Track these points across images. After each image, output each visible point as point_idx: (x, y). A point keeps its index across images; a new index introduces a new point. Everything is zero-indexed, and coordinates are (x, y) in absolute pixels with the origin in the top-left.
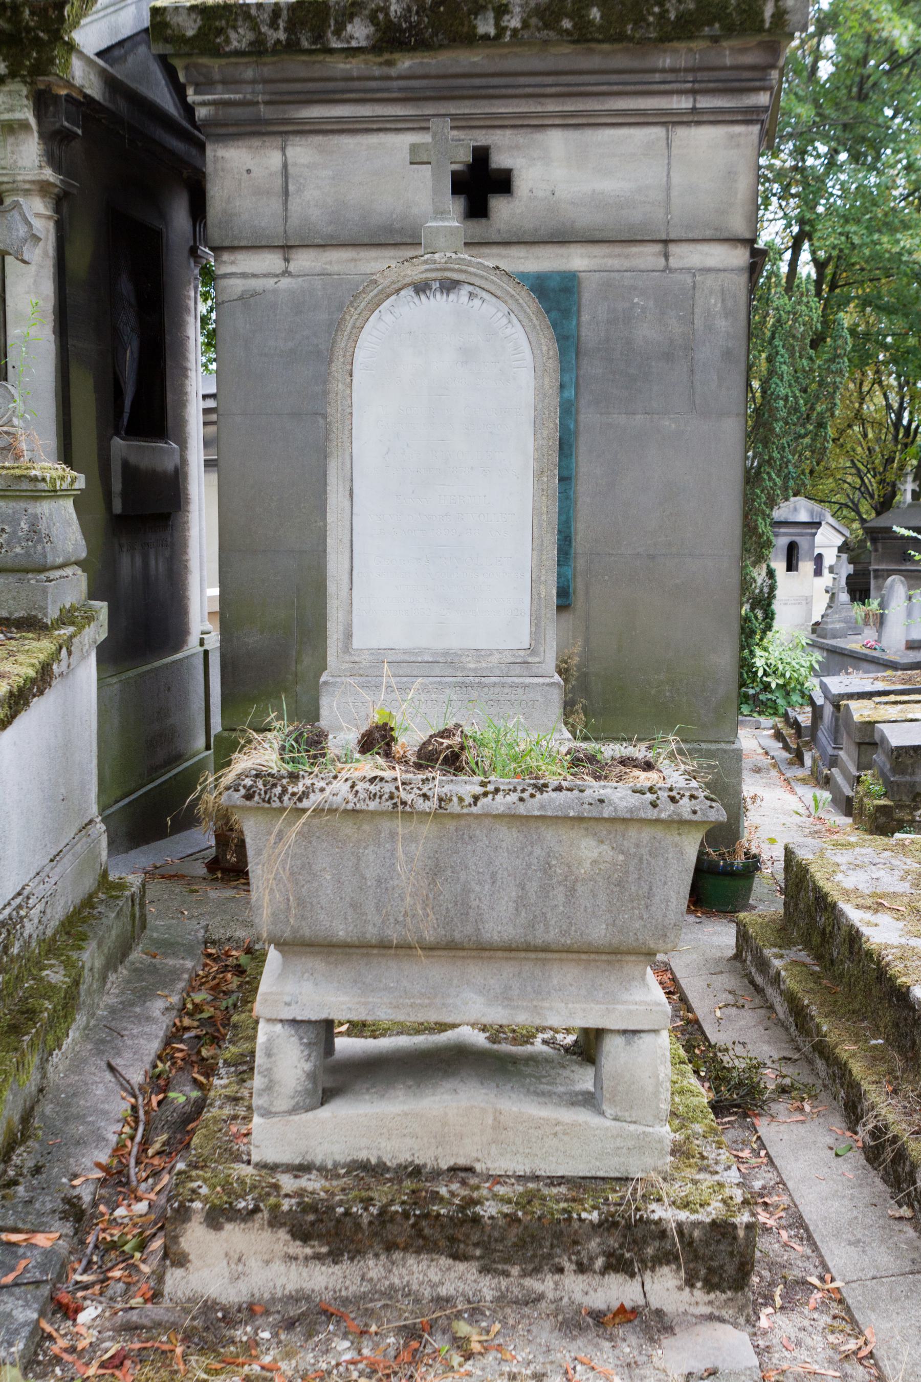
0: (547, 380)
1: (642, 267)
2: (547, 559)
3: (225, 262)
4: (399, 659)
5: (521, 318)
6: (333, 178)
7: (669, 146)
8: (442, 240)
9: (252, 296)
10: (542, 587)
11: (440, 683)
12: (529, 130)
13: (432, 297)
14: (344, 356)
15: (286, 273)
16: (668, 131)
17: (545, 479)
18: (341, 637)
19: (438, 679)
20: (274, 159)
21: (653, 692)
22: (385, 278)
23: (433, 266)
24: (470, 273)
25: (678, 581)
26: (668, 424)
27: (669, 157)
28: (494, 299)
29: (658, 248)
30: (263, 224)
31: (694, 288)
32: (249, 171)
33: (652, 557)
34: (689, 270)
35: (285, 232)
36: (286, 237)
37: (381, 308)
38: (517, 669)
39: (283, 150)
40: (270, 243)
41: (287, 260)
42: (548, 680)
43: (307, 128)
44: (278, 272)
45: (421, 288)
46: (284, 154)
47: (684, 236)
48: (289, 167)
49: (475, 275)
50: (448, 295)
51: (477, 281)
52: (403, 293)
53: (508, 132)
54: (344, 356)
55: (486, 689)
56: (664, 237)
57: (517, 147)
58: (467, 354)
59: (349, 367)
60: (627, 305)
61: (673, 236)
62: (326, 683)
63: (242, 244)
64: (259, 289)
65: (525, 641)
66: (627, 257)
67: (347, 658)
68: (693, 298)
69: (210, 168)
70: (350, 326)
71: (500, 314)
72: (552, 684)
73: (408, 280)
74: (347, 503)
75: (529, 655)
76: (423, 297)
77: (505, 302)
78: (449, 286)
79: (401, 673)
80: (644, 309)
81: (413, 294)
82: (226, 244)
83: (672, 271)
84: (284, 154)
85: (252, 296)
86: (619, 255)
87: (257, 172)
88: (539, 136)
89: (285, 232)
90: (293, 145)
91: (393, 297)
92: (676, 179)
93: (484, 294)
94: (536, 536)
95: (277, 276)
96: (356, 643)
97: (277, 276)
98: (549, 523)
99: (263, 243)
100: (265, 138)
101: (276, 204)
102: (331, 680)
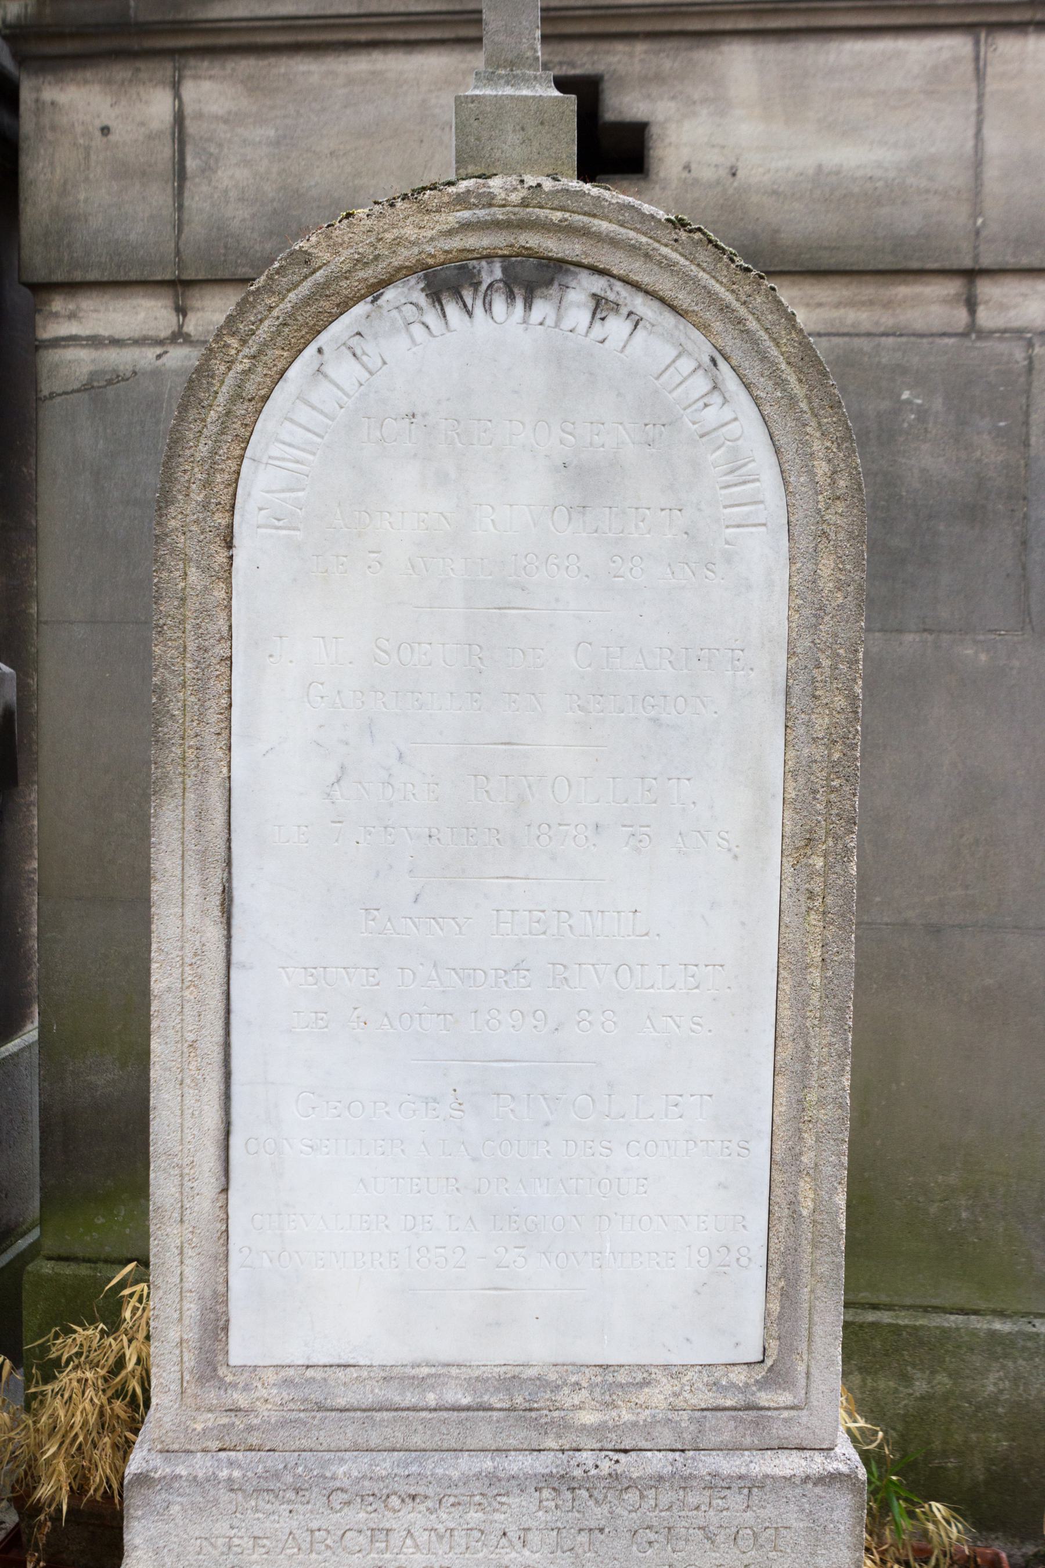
0: (827, 565)
1: (919, 326)
2: (821, 1103)
3: (56, 315)
4: (369, 1400)
5: (752, 375)
6: (278, 143)
7: (979, 75)
8: (513, 138)
9: (110, 382)
10: (805, 1186)
11: (493, 1479)
12: (684, 43)
13: (479, 311)
14: (207, 484)
15: (179, 337)
16: (977, 43)
17: (819, 863)
18: (192, 1335)
19: (487, 1464)
20: (157, 106)
21: (933, 1209)
22: (335, 248)
23: (482, 213)
24: (599, 238)
25: (989, 981)
26: (972, 654)
27: (980, 97)
28: (669, 319)
29: (952, 287)
30: (133, 237)
31: (1030, 369)
32: (105, 130)
33: (935, 930)
34: (1018, 333)
35: (178, 253)
36: (180, 264)
37: (323, 339)
38: (726, 1430)
39: (176, 87)
40: (146, 276)
41: (181, 311)
42: (818, 1464)
43: (225, 40)
44: (163, 334)
45: (447, 282)
46: (177, 95)
47: (1011, 261)
48: (188, 122)
49: (614, 242)
50: (528, 305)
51: (619, 262)
52: (390, 294)
53: (640, 48)
54: (207, 484)
55: (632, 1496)
56: (967, 263)
57: (659, 78)
58: (585, 483)
59: (220, 519)
60: (885, 405)
61: (986, 262)
62: (143, 1479)
63: (93, 276)
64: (125, 368)
65: (748, 1339)
66: (888, 305)
67: (212, 1396)
68: (1028, 392)
69: (27, 124)
70: (224, 392)
71: (686, 365)
72: (833, 1479)
73: (405, 256)
74: (214, 933)
75: (764, 1384)
76: (452, 309)
77: (704, 328)
78: (532, 277)
79: (375, 1440)
80: (923, 414)
81: (422, 299)
82: (59, 277)
83: (983, 334)
84: (177, 95)
85: (110, 382)
86: (871, 303)
87: (121, 133)
88: (705, 56)
89: (178, 253)
90: (196, 77)
91: (361, 309)
92: (995, 142)
93: (640, 304)
94: (787, 1031)
95: (160, 342)
96: (242, 1349)
97: (160, 342)
98: (828, 994)
99: (133, 276)
100: (140, 64)
101: (158, 197)
102: (162, 1468)
